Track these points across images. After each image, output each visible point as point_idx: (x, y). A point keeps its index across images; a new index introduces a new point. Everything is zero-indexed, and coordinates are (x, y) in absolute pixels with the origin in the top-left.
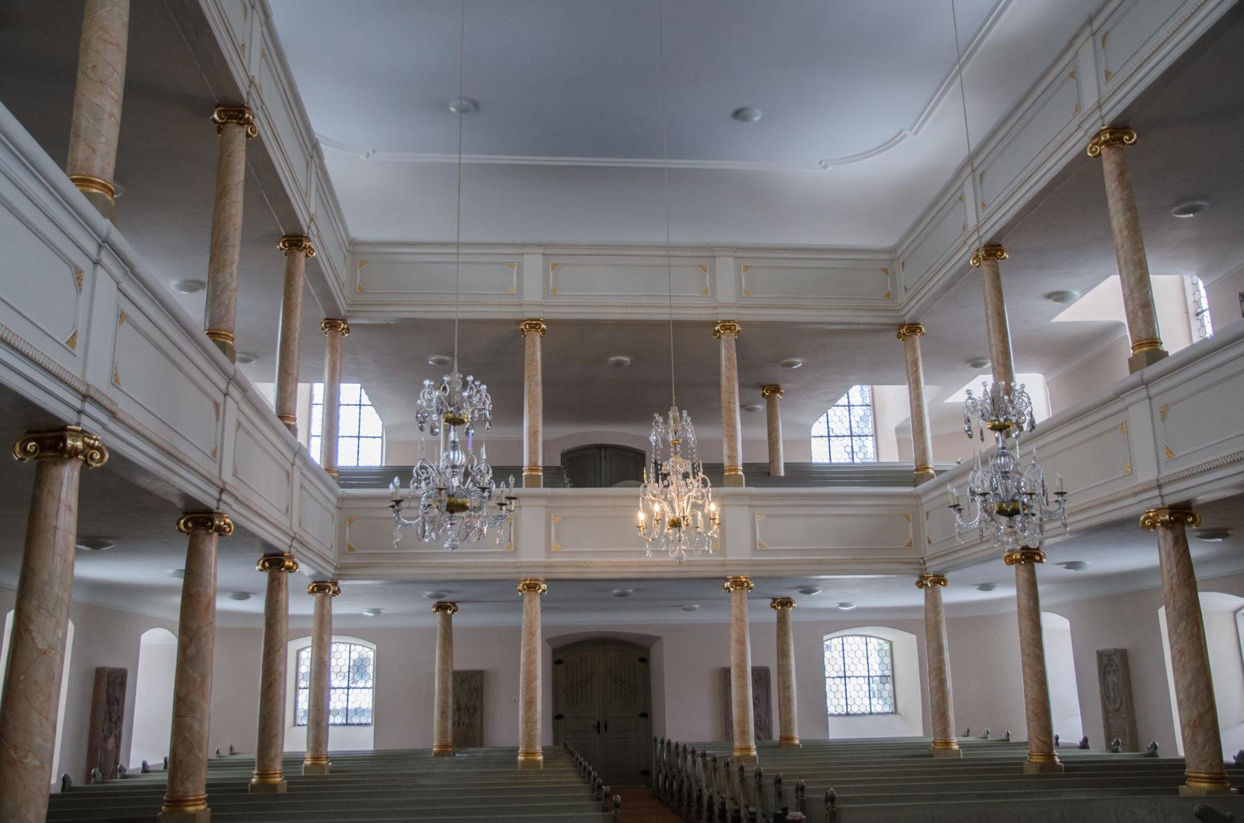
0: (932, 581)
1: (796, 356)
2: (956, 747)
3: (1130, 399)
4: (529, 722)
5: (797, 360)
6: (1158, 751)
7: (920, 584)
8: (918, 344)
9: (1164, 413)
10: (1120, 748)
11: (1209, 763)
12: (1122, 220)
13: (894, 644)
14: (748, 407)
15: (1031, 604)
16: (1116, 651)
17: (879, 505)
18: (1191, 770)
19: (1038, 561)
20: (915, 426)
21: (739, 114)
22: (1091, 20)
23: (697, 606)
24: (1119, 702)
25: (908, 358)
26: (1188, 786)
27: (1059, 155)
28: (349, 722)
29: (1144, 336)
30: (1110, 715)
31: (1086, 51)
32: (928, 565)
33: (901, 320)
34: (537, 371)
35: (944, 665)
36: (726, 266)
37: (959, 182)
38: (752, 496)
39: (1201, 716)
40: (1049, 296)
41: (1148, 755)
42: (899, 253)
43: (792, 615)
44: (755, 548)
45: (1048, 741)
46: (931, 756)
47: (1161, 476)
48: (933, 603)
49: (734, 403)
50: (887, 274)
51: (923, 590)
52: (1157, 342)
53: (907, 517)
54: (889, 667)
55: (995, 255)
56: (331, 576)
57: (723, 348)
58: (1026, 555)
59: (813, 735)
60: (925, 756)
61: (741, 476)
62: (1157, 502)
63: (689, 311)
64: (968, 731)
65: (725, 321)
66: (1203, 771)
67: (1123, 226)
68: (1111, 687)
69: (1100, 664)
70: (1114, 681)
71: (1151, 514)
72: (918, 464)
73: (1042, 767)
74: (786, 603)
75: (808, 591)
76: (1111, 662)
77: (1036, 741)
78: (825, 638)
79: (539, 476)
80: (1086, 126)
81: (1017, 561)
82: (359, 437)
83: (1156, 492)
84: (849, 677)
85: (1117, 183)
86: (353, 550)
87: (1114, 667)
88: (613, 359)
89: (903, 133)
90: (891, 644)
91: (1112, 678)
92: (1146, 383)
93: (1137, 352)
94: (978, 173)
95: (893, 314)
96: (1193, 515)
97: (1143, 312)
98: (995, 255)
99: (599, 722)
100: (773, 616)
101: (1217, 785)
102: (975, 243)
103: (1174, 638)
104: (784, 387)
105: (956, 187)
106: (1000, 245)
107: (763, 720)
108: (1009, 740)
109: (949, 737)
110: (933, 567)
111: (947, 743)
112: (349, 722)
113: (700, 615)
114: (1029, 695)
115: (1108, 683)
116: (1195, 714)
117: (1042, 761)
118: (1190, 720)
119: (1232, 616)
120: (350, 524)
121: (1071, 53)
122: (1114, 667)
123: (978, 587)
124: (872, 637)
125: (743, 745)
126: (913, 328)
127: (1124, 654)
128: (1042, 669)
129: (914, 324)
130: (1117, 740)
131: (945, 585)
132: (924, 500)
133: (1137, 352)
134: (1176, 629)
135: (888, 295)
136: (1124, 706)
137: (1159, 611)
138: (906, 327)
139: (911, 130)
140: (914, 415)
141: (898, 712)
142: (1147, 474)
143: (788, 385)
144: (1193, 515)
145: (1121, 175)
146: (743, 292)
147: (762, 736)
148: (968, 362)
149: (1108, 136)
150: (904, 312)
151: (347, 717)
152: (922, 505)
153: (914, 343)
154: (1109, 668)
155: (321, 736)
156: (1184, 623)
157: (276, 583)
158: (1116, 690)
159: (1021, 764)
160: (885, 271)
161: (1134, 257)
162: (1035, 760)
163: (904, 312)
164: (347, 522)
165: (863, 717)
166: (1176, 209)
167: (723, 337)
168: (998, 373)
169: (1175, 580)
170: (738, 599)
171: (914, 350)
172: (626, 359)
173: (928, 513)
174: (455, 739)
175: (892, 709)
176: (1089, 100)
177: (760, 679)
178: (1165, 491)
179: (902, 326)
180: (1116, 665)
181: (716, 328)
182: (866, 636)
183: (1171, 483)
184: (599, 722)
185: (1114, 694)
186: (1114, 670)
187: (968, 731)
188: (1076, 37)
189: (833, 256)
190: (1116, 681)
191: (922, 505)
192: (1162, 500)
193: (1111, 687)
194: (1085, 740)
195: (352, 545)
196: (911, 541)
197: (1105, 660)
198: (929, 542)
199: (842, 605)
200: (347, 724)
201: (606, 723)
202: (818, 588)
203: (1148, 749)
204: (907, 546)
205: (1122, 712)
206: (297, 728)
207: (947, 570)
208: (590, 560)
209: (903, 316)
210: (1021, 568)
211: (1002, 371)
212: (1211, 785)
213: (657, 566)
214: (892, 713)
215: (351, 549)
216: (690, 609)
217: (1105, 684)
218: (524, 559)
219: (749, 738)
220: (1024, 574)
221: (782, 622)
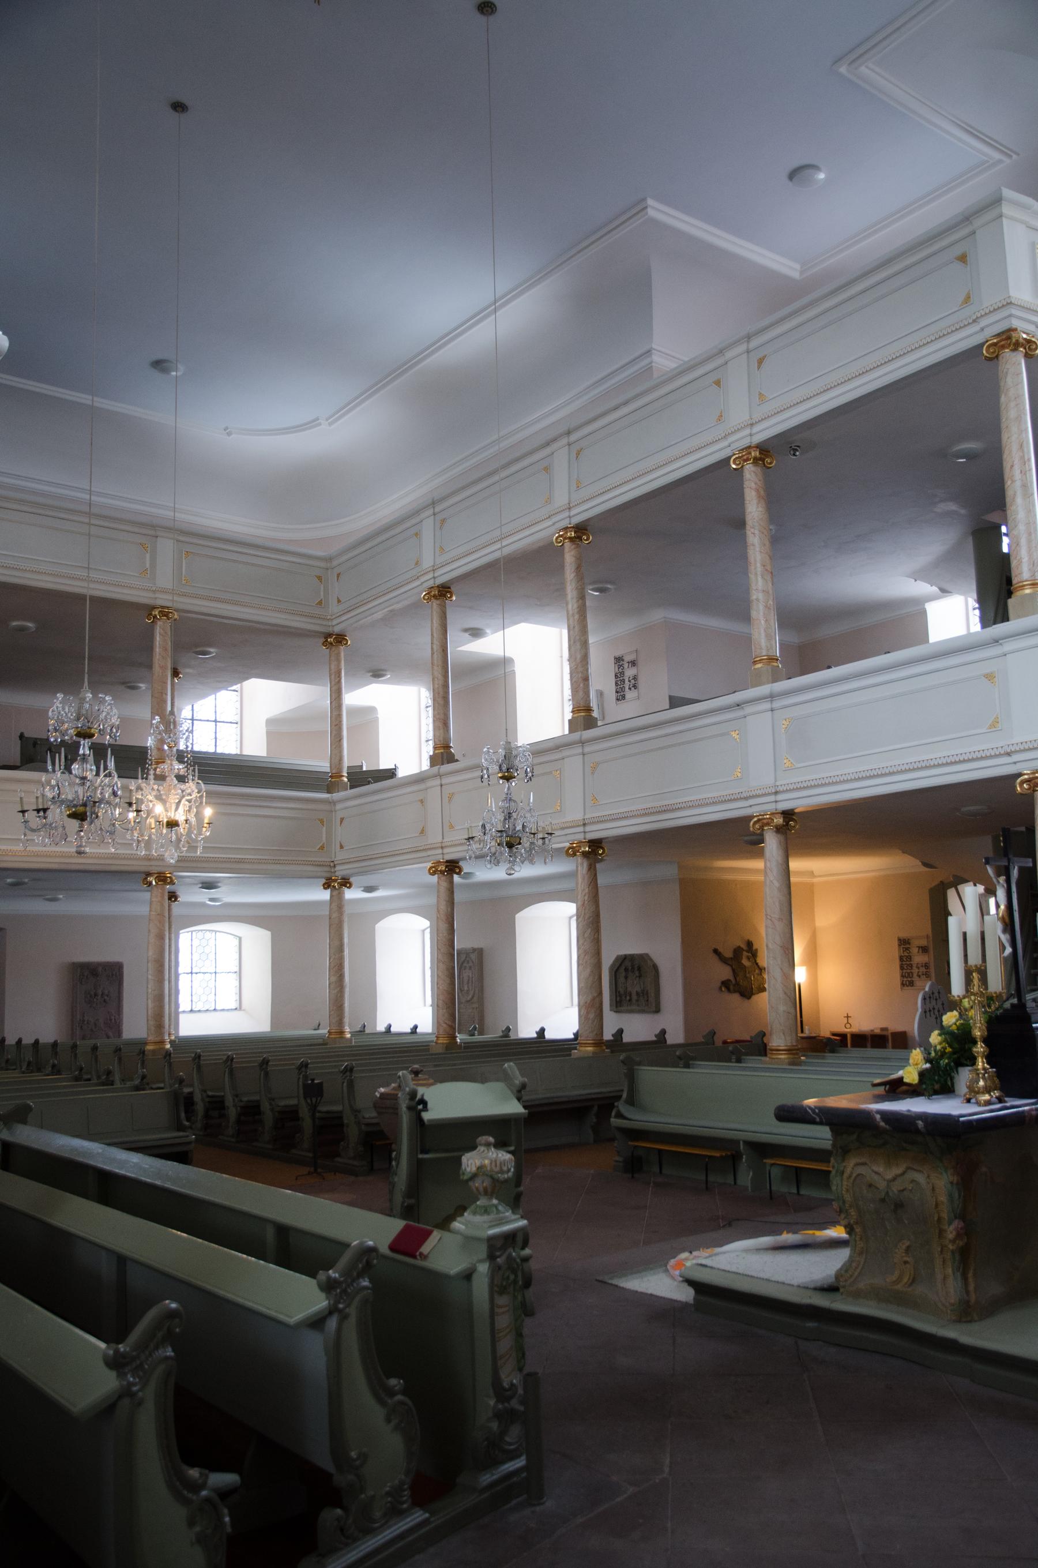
0: (336, 883)
1: (210, 646)
2: (348, 1036)
3: (566, 753)
7: (327, 886)
8: (342, 654)
9: (594, 769)
10: (476, 1032)
11: (595, 1033)
12: (575, 606)
13: (243, 939)
14: (129, 685)
16: (474, 950)
17: (302, 809)
18: (582, 1038)
20: (333, 735)
21: (159, 365)
22: (569, 433)
23: (61, 896)
24: (470, 996)
25: (333, 667)
26: (579, 1050)
27: (527, 532)
29: (582, 704)
31: (561, 458)
32: (338, 868)
33: (330, 630)
35: (344, 962)
36: (166, 548)
39: (594, 999)
40: (466, 630)
41: (501, 1037)
42: (335, 563)
45: (453, 1025)
46: (326, 1044)
47: (587, 817)
49: (166, 694)
52: (591, 710)
53: (322, 821)
55: (445, 596)
57: (158, 634)
60: (322, 1044)
62: (581, 837)
63: (126, 591)
64: (319, 1025)
65: (163, 607)
67: (576, 611)
68: (466, 981)
70: (469, 976)
71: (575, 845)
72: (334, 771)
77: (445, 1025)
78: (181, 932)
80: (555, 519)
83: (581, 829)
85: (575, 574)
87: (471, 964)
88: (14, 623)
90: (240, 939)
91: (467, 973)
92: (582, 743)
93: (576, 715)
94: (439, 517)
95: (324, 623)
96: (603, 848)
97: (584, 684)
98: (445, 596)
101: (598, 1048)
102: (428, 581)
103: (581, 942)
105: (414, 521)
107: (113, 1018)
108: (364, 1031)
110: (341, 871)
111: (342, 1032)
113: (67, 906)
114: (441, 988)
116: (590, 998)
117: (447, 1042)
119: (567, 921)
121: (548, 451)
122: (471, 964)
123: (362, 889)
125: (158, 1039)
126: (340, 639)
127: (480, 952)
129: (341, 635)
131: (349, 888)
132: (339, 806)
133: (576, 715)
134: (584, 935)
135: (320, 603)
137: (517, 916)
139: (327, 420)
142: (575, 814)
143: (188, 670)
144: (603, 848)
145: (578, 568)
146: (183, 579)
147: (111, 1034)
148: (369, 672)
149: (573, 534)
150: (335, 622)
152: (335, 811)
153: (338, 654)
156: (589, 930)
158: (470, 984)
159: (429, 1046)
160: (320, 578)
161: (582, 638)
162: (441, 1042)
163: (335, 622)
165: (208, 1014)
166: (591, 587)
167: (159, 623)
168: (438, 703)
169: (586, 898)
170: (159, 895)
171: (339, 661)
172: (30, 625)
173: (342, 820)
176: (561, 499)
177: (113, 975)
178: (588, 828)
179: (330, 635)
182: (216, 932)
183: (593, 823)
185: (468, 987)
187: (319, 1025)
188: (554, 440)
189: (273, 556)
191: (335, 811)
192: (585, 836)
193: (466, 981)
196: (324, 844)
198: (342, 847)
204: (319, 849)
207: (353, 875)
208: (9, 848)
209: (333, 626)
210: (443, 878)
211: (442, 702)
213: (128, 859)
216: (54, 900)
219: (164, 1033)
220: (444, 884)
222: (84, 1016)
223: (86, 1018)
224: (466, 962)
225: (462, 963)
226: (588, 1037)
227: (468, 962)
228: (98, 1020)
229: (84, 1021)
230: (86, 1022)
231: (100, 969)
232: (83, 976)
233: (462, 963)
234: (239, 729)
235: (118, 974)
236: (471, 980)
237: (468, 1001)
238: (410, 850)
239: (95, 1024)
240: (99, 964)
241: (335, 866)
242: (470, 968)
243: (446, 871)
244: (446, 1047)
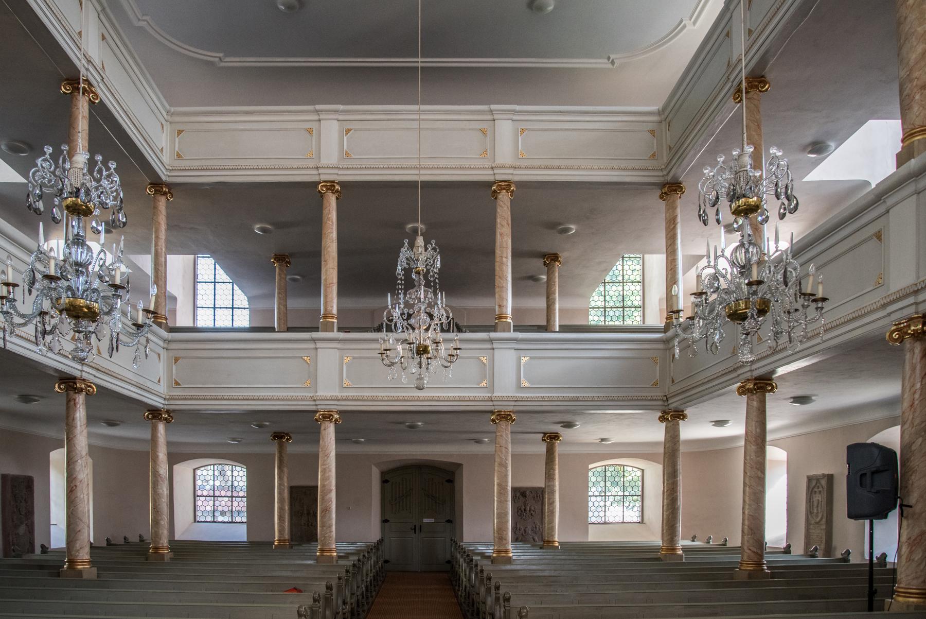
4: (324, 526)
5: (572, 226)
6: (851, 557)
7: (662, 419)
13: (645, 471)
15: (758, 430)
16: (824, 475)
18: (902, 585)
19: (770, 391)
24: (819, 518)
28: (234, 520)
30: (811, 527)
34: (332, 229)
37: (728, 15)
38: (517, 340)
43: (559, 449)
44: (519, 387)
48: (673, 437)
50: (654, 136)
51: (664, 424)
54: (640, 488)
56: (162, 406)
58: (759, 385)
59: (574, 538)
61: (510, 322)
62: (910, 311)
66: (914, 587)
68: (815, 504)
69: (808, 487)
70: (818, 500)
73: (751, 575)
74: (554, 437)
75: (569, 425)
76: (818, 485)
79: (334, 322)
81: (750, 391)
82: (233, 308)
84: (608, 496)
86: (179, 384)
89: (683, 23)
90: (643, 471)
91: (817, 498)
99: (415, 526)
100: (542, 448)
104: (563, 256)
106: (763, 76)
109: (675, 545)
110: (674, 404)
112: (234, 520)
115: (813, 502)
118: (910, 538)
120: (176, 362)
124: (629, 466)
127: (832, 475)
128: (762, 490)
130: (816, 547)
136: (824, 520)
138: (668, 186)
139: (690, 20)
140: (669, 268)
141: (644, 522)
147: (536, 538)
151: (232, 517)
154: (816, 490)
155: (160, 532)
157: (72, 403)
158: (819, 507)
164: (173, 361)
174: (292, 539)
175: (639, 520)
177: (537, 496)
180: (823, 487)
181: (493, 188)
184: (415, 526)
185: (817, 510)
186: (820, 492)
190: (820, 500)
193: (815, 504)
194: (789, 546)
195: (178, 380)
197: (814, 483)
199: (602, 440)
200: (232, 522)
201: (421, 526)
202: (577, 423)
203: (842, 554)
205: (822, 524)
206: (197, 524)
212: (921, 600)
214: (640, 522)
215: (177, 383)
217: (810, 502)
218: (321, 393)
221: (550, 452)
222: (517, 525)
223: (518, 526)
224: (816, 487)
225: (813, 489)
226: (909, 584)
227: (818, 488)
228: (527, 527)
229: (517, 528)
230: (518, 529)
231: (528, 493)
232: (516, 497)
233: (813, 489)
234: (642, 311)
235: (541, 496)
236: (820, 503)
237: (816, 523)
238: (722, 373)
239: (525, 530)
240: (527, 488)
241: (667, 400)
242: (820, 492)
243: (755, 390)
244: (749, 574)
